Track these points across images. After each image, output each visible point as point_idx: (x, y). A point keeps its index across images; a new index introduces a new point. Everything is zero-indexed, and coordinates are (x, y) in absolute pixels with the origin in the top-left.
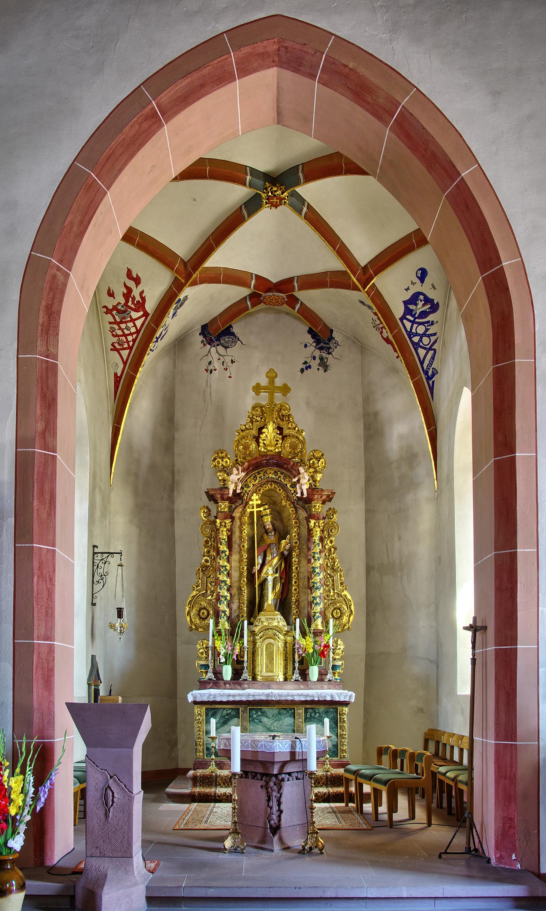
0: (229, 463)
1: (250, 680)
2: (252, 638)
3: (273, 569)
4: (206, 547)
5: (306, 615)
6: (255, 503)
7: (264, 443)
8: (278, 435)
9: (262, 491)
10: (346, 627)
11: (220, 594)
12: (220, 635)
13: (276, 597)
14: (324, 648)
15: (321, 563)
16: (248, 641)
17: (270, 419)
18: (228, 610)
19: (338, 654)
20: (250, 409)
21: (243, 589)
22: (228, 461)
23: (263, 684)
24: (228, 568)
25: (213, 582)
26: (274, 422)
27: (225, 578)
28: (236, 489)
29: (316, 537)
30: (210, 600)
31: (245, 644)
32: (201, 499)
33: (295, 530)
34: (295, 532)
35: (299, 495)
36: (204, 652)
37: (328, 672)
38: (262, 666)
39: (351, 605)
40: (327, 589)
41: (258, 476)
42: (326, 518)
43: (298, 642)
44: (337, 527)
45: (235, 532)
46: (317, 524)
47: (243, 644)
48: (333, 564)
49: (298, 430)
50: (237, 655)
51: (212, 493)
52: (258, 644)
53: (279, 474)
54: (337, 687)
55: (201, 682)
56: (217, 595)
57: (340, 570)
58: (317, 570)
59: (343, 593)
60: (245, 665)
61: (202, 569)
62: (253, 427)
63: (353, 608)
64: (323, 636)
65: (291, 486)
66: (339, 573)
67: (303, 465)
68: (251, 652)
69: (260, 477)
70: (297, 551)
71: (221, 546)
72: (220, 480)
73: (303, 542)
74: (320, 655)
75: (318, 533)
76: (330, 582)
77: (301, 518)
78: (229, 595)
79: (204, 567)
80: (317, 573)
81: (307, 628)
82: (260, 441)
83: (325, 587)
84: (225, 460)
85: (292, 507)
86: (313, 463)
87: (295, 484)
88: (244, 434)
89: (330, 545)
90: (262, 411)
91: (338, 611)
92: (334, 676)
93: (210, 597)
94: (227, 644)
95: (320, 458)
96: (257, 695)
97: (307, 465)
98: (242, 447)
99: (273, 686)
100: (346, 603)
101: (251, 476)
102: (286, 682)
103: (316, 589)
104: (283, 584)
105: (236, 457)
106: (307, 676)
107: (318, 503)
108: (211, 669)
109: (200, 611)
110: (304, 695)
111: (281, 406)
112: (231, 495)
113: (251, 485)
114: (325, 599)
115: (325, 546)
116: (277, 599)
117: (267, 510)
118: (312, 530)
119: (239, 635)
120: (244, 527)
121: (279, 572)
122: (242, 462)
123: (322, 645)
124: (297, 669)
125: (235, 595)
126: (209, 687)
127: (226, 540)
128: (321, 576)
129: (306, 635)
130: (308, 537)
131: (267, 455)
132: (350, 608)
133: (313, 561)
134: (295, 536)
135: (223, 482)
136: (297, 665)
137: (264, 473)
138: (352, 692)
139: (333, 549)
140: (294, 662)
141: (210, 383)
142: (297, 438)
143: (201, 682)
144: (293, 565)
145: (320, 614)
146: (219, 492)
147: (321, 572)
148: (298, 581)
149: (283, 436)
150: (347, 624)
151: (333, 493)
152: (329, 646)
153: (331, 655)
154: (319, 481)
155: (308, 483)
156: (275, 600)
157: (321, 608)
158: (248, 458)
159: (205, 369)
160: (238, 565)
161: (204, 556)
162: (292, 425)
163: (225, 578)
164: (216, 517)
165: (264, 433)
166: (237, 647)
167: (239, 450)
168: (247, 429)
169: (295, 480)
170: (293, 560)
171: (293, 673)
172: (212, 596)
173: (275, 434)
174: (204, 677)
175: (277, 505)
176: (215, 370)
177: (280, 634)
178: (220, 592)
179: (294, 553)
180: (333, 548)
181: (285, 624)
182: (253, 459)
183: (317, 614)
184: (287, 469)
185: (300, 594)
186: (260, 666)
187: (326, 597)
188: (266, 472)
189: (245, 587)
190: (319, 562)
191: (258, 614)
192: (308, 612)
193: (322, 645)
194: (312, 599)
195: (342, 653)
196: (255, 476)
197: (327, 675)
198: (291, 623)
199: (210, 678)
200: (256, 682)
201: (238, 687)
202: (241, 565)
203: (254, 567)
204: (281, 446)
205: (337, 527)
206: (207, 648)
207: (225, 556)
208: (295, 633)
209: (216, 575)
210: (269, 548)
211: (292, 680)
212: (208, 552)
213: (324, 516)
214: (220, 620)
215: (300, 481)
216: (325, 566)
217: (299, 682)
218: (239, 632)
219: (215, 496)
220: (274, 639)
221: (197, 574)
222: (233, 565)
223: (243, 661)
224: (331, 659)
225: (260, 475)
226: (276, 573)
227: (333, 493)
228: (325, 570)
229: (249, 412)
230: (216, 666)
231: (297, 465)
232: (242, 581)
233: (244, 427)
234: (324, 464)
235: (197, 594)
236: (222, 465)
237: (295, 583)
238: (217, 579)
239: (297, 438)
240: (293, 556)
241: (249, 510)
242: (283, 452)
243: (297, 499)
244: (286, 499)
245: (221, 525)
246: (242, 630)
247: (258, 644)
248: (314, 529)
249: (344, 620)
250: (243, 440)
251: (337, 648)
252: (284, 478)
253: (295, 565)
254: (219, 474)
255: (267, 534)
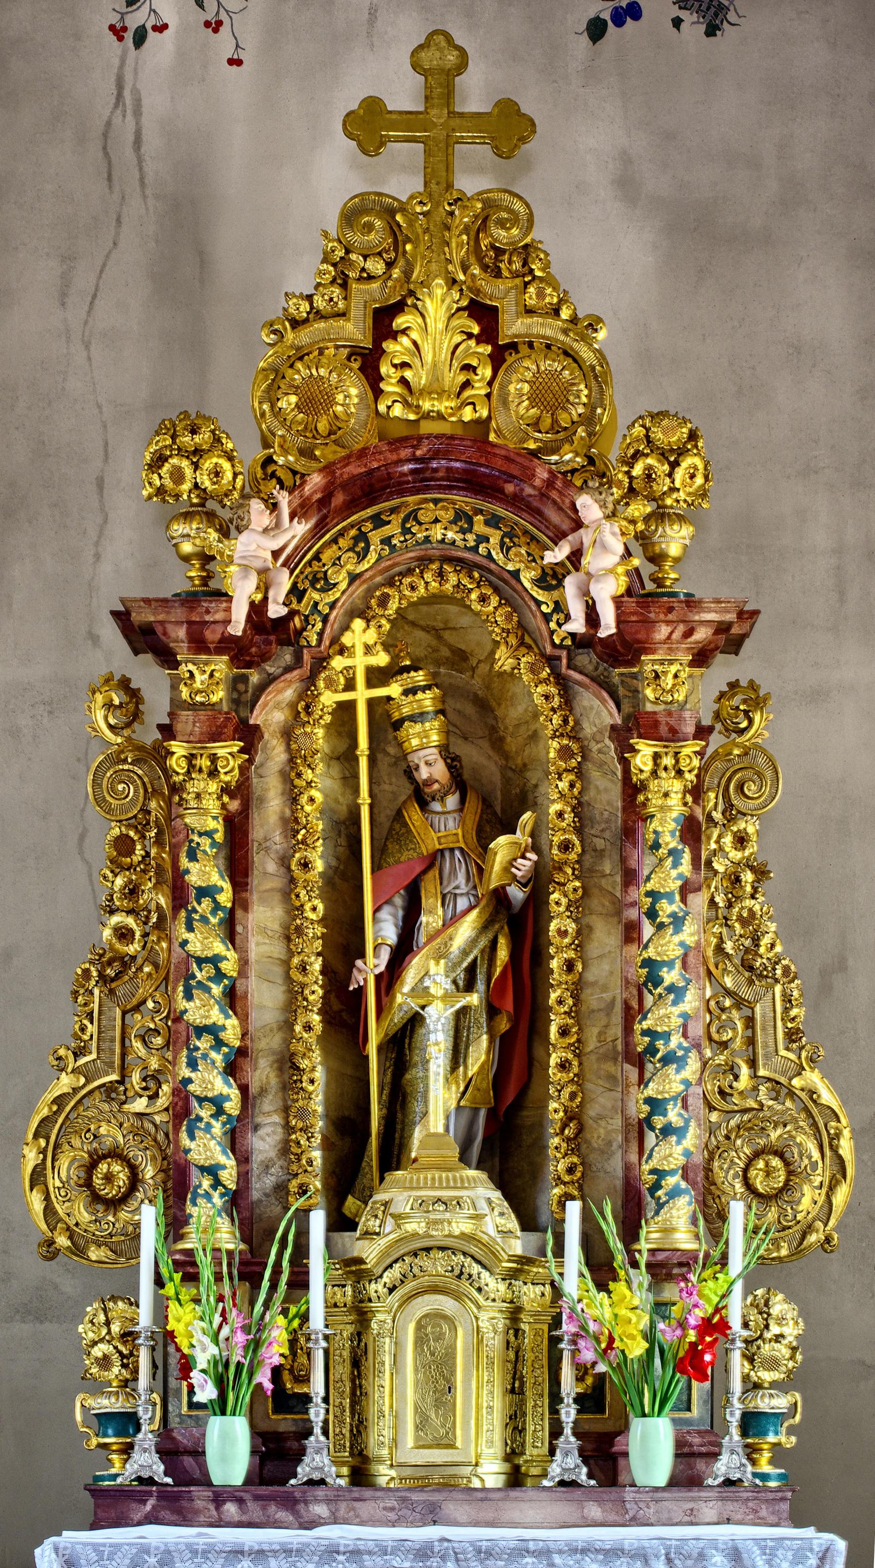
0: (229, 475)
1: (342, 1482)
2: (349, 1290)
3: (451, 968)
4: (117, 867)
5: (619, 1183)
6: (360, 662)
7: (403, 381)
8: (472, 342)
9: (393, 605)
10: (813, 1238)
11: (191, 1088)
12: (191, 1277)
13: (473, 1100)
14: (701, 1334)
15: (690, 941)
16: (331, 1306)
17: (434, 267)
18: (230, 1162)
19: (772, 1364)
20: (333, 228)
21: (304, 1064)
22: (226, 465)
23: (404, 1500)
24: (229, 967)
25: (157, 1032)
26: (453, 282)
27: (216, 1016)
28: (265, 599)
29: (662, 822)
30: (140, 1115)
31: (317, 1321)
32: (94, 639)
33: (563, 785)
34: (562, 795)
35: (578, 625)
36: (116, 1358)
37: (720, 1445)
38: (397, 1417)
39: (838, 1136)
40: (721, 1059)
41: (375, 537)
42: (710, 729)
43: (572, 1310)
44: (768, 774)
45: (262, 800)
46: (668, 761)
47: (305, 1318)
48: (748, 943)
49: (574, 320)
50: (277, 1371)
51: (143, 616)
52: (380, 1320)
53: (480, 526)
54: (764, 1513)
55: (97, 1492)
56: (176, 1092)
57: (786, 970)
58: (670, 976)
59: (797, 1082)
60: (316, 1414)
61: (101, 975)
62: (348, 307)
63: (846, 1147)
64: (693, 1278)
65: (542, 582)
66: (778, 989)
67: (594, 484)
68: (346, 1354)
69: (386, 541)
70: (570, 886)
71: (194, 867)
72: (186, 559)
73: (600, 843)
74: (680, 1367)
75: (675, 800)
76: (734, 1029)
77: (588, 729)
78: (234, 1093)
79: (110, 963)
80: (671, 989)
81: (616, 1244)
82: (385, 369)
83: (708, 1053)
84: (208, 464)
85: (546, 681)
86: (649, 476)
87: (560, 570)
88: (304, 337)
89: (736, 855)
90: (394, 230)
91: (776, 1162)
92: (754, 1462)
93: (144, 1101)
94: (225, 1320)
95: (682, 452)
96: (370, 1553)
97: (620, 484)
98: (293, 399)
99: (451, 1508)
100: (815, 1125)
101: (341, 534)
102: (515, 1493)
103: (667, 1060)
104: (503, 1037)
105: (266, 445)
106: (621, 1462)
107: (671, 662)
108: (146, 1437)
109: (92, 1167)
110: (598, 1551)
111: (489, 205)
112: (238, 626)
113: (341, 579)
114: (711, 1108)
115: (709, 863)
116: (476, 1111)
117: (420, 696)
118: (643, 787)
119: (284, 1278)
120: (309, 775)
121: (481, 985)
122: (294, 473)
123: (692, 1321)
124: (568, 1431)
125: (263, 1091)
126: (137, 1517)
127: (219, 837)
128: (690, 1002)
129: (615, 1279)
130: (625, 822)
131: (420, 438)
132: (834, 1149)
133: (648, 930)
134: (560, 815)
135: (203, 568)
136: (569, 1414)
137: (405, 520)
138: (831, 1536)
139: (748, 877)
140: (555, 1398)
141: (136, 92)
142: (566, 354)
143: (97, 1492)
144: (552, 950)
145: (685, 1177)
146: (179, 613)
147: (689, 981)
148: (578, 1023)
149: (495, 345)
150: (819, 1225)
151: (748, 616)
152: (723, 1326)
153: (738, 1365)
154: (677, 560)
155: (621, 570)
156: (465, 1116)
157: (687, 1153)
158: (325, 453)
159: (112, 28)
160: (277, 949)
161: (112, 912)
162: (541, 295)
163: (216, 1016)
164: (168, 731)
165: (404, 332)
166: (275, 1333)
167: (277, 413)
168: (320, 315)
169: (558, 554)
170: (553, 926)
171: (552, 1452)
172: (153, 1097)
173: (458, 338)
174: (113, 1471)
175: (473, 669)
176: (161, 28)
177: (485, 1274)
178: (190, 1081)
179: (555, 896)
180: (752, 869)
181: (512, 1223)
182: (348, 457)
183: (671, 1181)
184: (517, 502)
185: (589, 1086)
186: (388, 1420)
187: (716, 1100)
188: (413, 515)
189: (317, 1055)
190: (677, 939)
191: (382, 1179)
192: (628, 1167)
193: (692, 1321)
194: (646, 1108)
195: (792, 1358)
196: (362, 537)
197: (714, 1456)
198: (544, 1218)
199: (145, 1474)
200: (367, 1493)
201: (282, 1515)
202: (291, 954)
203: (359, 963)
204: (488, 396)
205: (768, 774)
206: (128, 1336)
207: (214, 912)
208: (561, 1265)
209: (170, 1000)
210: (434, 873)
211: (546, 1483)
212: (133, 891)
213: (707, 722)
214: (190, 1209)
215: (584, 562)
216: (710, 952)
217: (578, 1493)
218: (285, 1263)
219: (159, 630)
220: (458, 1296)
221: (75, 994)
222: (253, 954)
223: (306, 1399)
224: (737, 1386)
225: (386, 531)
226: (469, 987)
227: (748, 616)
228: (709, 973)
229: (326, 234)
230: (174, 1421)
231: (568, 484)
232: (298, 1028)
233: (305, 306)
234: (699, 480)
235: (75, 1090)
236: (196, 486)
237: (564, 1032)
238: (178, 1019)
239: (566, 354)
240: (553, 908)
241: (329, 699)
242: (500, 421)
243: (568, 642)
244: (513, 640)
245: (191, 767)
246: (301, 1251)
247: (380, 1317)
248: (653, 785)
249: (806, 1203)
250: (299, 365)
251: (768, 1335)
252: (502, 544)
253: (559, 949)
254: (179, 528)
255: (424, 805)
